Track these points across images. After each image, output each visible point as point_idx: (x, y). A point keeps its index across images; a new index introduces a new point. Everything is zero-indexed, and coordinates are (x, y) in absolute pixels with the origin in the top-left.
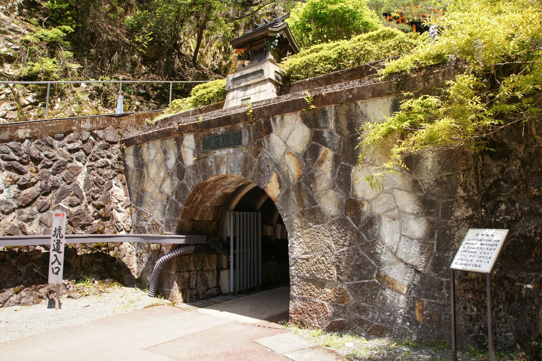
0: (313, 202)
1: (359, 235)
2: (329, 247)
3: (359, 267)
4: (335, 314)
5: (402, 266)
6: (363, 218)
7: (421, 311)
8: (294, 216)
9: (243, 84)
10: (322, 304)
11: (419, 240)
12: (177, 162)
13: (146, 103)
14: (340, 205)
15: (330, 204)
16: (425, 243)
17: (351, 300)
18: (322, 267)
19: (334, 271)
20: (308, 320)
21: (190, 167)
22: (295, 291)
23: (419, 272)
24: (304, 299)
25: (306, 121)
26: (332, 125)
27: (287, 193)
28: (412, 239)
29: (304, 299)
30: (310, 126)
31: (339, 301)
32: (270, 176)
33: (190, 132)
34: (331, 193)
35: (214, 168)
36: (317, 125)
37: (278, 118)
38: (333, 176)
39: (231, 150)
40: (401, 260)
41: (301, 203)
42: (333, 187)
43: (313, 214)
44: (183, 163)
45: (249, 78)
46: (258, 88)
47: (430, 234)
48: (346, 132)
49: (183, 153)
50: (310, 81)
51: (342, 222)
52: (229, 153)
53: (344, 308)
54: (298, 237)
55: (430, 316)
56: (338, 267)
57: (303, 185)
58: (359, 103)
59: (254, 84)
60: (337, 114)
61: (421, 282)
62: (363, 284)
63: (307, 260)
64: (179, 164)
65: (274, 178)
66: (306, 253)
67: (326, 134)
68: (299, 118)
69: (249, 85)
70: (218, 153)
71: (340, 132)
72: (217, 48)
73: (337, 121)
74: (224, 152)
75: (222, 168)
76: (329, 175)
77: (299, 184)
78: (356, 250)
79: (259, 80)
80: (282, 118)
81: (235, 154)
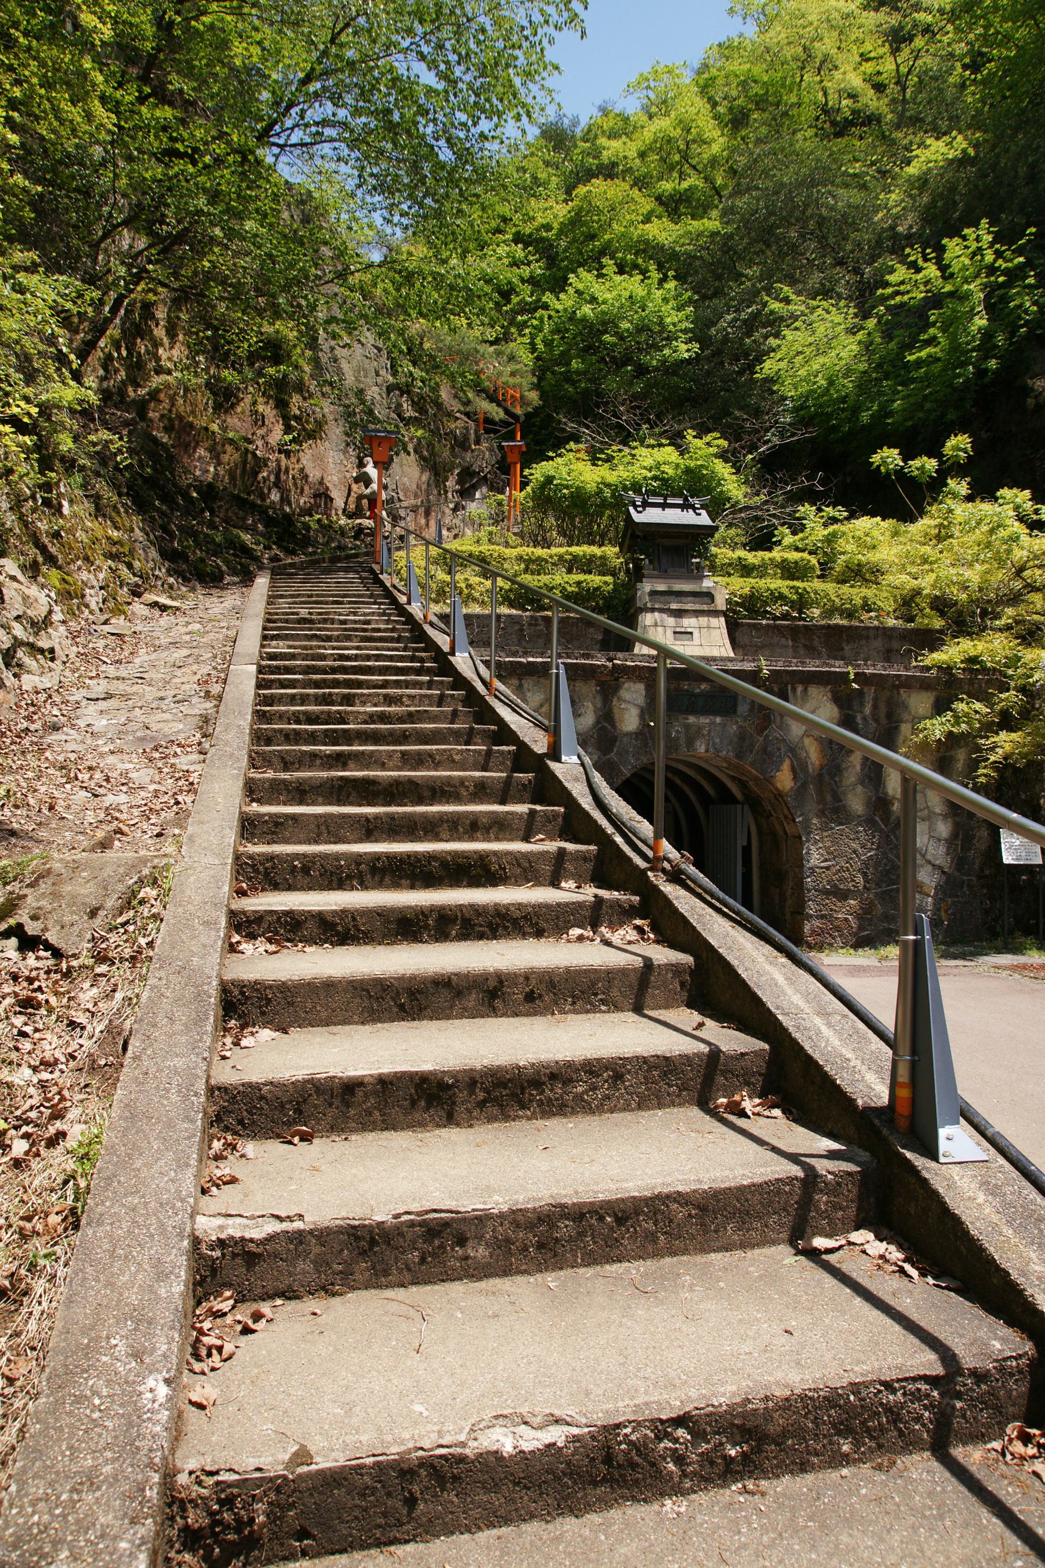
0: (837, 798)
1: (888, 836)
2: (855, 852)
3: (888, 872)
4: (861, 928)
5: (929, 868)
6: (893, 818)
7: (946, 911)
8: (811, 815)
9: (674, 606)
10: (846, 919)
11: (946, 840)
12: (598, 722)
13: (163, 514)
14: (868, 804)
15: (856, 803)
16: (950, 842)
17: (879, 909)
18: (846, 875)
19: (860, 879)
20: (829, 940)
21: (628, 734)
22: (811, 908)
23: (944, 872)
24: (823, 917)
25: (836, 699)
26: (867, 710)
27: (805, 785)
28: (939, 840)
29: (823, 917)
30: (840, 707)
31: (864, 915)
32: (781, 762)
33: (640, 679)
34: (859, 789)
35: (682, 741)
36: (850, 708)
37: (800, 689)
38: (862, 769)
39: (718, 720)
40: (929, 862)
41: (821, 800)
42: (862, 783)
43: (835, 812)
44: (613, 724)
45: (684, 599)
46: (703, 620)
47: (954, 835)
48: (884, 721)
49: (616, 710)
50: (767, 625)
51: (869, 822)
52: (713, 723)
53: (871, 920)
54: (816, 842)
55: (954, 914)
56: (864, 875)
57: (827, 778)
58: (902, 691)
59: (695, 611)
60: (876, 700)
61: (946, 883)
62: (891, 890)
63: (828, 868)
64: (603, 728)
65: (786, 766)
66: (826, 860)
67: (859, 719)
68: (829, 695)
69: (686, 611)
70: (692, 719)
71: (876, 721)
72: (112, 345)
73: (875, 707)
74: (704, 720)
75: (698, 743)
76: (858, 768)
77: (820, 776)
78: (884, 854)
79: (705, 607)
80: (805, 690)
81: (723, 725)
